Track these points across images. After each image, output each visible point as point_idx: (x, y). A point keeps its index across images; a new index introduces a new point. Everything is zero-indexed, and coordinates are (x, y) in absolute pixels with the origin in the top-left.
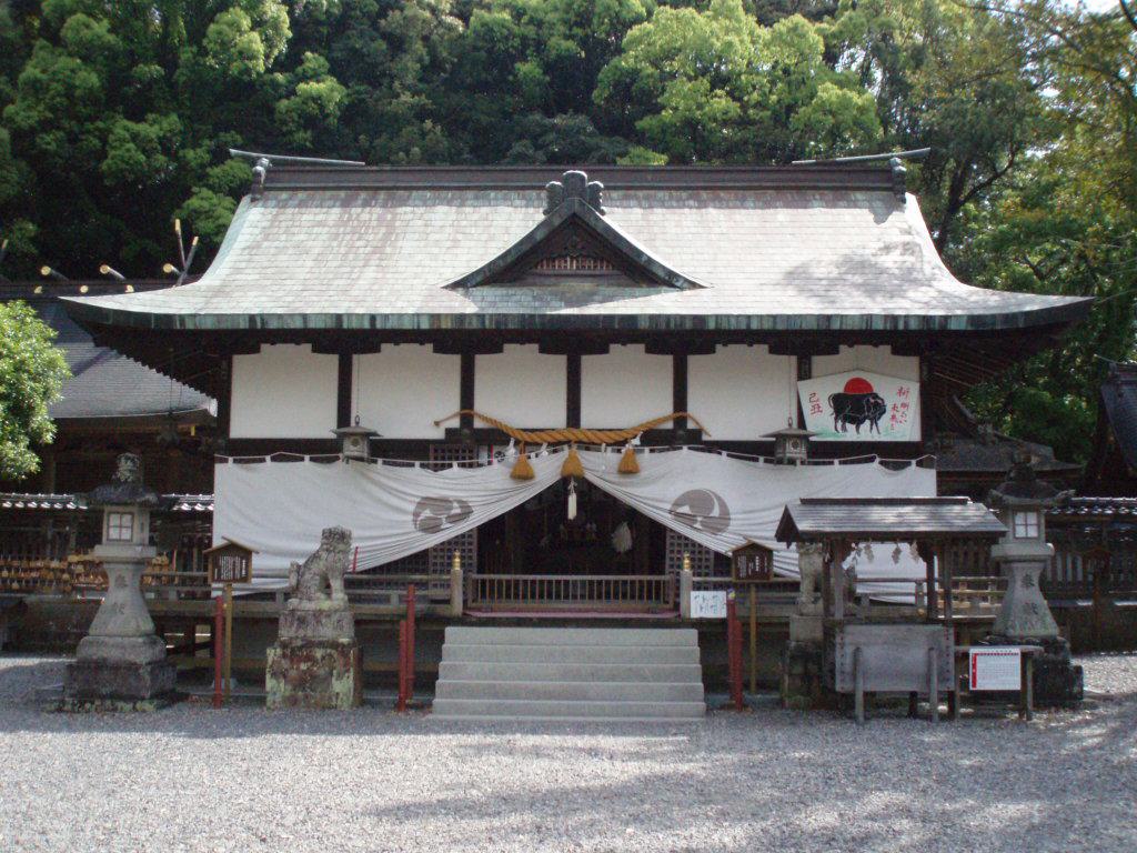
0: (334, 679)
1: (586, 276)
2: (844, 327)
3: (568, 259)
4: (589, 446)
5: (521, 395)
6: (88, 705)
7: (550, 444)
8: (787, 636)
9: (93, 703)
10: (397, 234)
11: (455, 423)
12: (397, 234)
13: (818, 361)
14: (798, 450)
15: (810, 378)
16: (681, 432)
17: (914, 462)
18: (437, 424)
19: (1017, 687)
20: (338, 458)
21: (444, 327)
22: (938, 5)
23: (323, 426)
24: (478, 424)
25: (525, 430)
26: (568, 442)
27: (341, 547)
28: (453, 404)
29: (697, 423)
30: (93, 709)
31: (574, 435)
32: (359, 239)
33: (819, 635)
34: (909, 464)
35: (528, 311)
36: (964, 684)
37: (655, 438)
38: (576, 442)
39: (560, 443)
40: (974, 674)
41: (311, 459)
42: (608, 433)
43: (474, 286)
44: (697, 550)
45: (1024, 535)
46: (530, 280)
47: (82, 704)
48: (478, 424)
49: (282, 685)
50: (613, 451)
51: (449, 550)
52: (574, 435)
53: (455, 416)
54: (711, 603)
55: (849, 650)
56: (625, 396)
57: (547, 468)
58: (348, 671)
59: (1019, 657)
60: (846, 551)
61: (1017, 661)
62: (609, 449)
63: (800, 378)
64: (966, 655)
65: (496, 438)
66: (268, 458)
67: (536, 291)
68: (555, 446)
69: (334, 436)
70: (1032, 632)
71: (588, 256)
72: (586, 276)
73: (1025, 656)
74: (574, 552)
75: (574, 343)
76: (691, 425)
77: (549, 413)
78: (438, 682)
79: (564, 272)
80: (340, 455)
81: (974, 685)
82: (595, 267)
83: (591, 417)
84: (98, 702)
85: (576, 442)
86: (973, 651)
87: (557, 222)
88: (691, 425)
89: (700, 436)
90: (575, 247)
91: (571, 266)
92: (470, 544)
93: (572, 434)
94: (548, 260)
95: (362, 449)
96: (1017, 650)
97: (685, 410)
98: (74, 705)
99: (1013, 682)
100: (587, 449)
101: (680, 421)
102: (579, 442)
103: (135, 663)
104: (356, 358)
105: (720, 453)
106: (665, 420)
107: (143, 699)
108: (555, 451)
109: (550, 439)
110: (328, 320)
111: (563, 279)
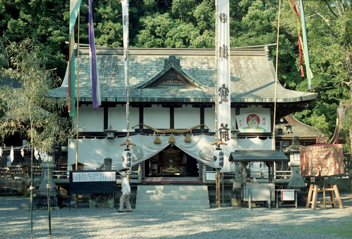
0: (108, 200)
1: (175, 85)
2: (248, 102)
3: (170, 80)
4: (176, 134)
5: (157, 121)
6: (40, 208)
7: (165, 133)
8: (232, 187)
9: (42, 207)
10: (119, 70)
11: (138, 128)
12: (119, 70)
13: (241, 109)
14: (111, 135)
15: (239, 114)
16: (202, 130)
17: (268, 137)
18: (133, 128)
19: (293, 200)
20: (105, 138)
21: (136, 101)
22: (236, 63)
23: (101, 130)
24: (144, 128)
25: (158, 129)
26: (170, 133)
27: (110, 163)
28: (137, 122)
29: (207, 127)
30: (42, 209)
31: (171, 132)
32: (108, 72)
33: (240, 186)
34: (267, 138)
35: (160, 97)
36: (279, 199)
37: (196, 132)
38: (173, 133)
39: (168, 133)
40: (282, 196)
41: (97, 138)
42: (182, 130)
43: (144, 88)
44: (208, 167)
45: (296, 160)
46: (159, 86)
47: (39, 208)
48: (144, 128)
49: (94, 202)
50: (183, 135)
51: (137, 166)
52: (171, 132)
53: (138, 125)
54: (212, 176)
55: (247, 190)
56: (186, 121)
57: (165, 142)
58: (112, 197)
59: (294, 192)
60: (247, 164)
61: (293, 193)
62: (182, 135)
63: (236, 114)
64: (280, 192)
65: (149, 131)
66: (95, 137)
67: (162, 90)
68: (167, 134)
69: (103, 131)
70: (298, 186)
71: (176, 79)
72: (175, 85)
73: (295, 191)
74: (174, 164)
75: (173, 106)
76: (205, 128)
77: (166, 126)
78: (136, 200)
79: (169, 84)
80: (106, 137)
81: (282, 199)
82: (178, 83)
83: (178, 125)
84: (43, 207)
85: (173, 133)
86: (282, 190)
87: (167, 70)
88: (205, 128)
89: (208, 131)
90: (172, 77)
91: (171, 82)
92: (143, 164)
93: (172, 131)
94: (165, 81)
95: (112, 135)
96: (293, 190)
97: (143, 123)
98: (36, 208)
99: (292, 198)
100: (176, 135)
101: (202, 127)
102: (174, 133)
103: (53, 196)
104: (109, 108)
105: (148, 135)
106: (198, 127)
107: (56, 206)
108: (167, 135)
109: (166, 132)
110: (103, 99)
111: (170, 86)
